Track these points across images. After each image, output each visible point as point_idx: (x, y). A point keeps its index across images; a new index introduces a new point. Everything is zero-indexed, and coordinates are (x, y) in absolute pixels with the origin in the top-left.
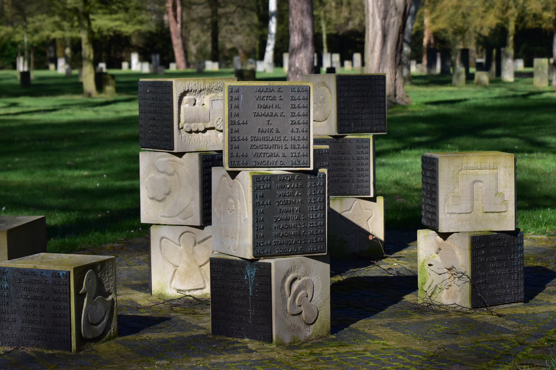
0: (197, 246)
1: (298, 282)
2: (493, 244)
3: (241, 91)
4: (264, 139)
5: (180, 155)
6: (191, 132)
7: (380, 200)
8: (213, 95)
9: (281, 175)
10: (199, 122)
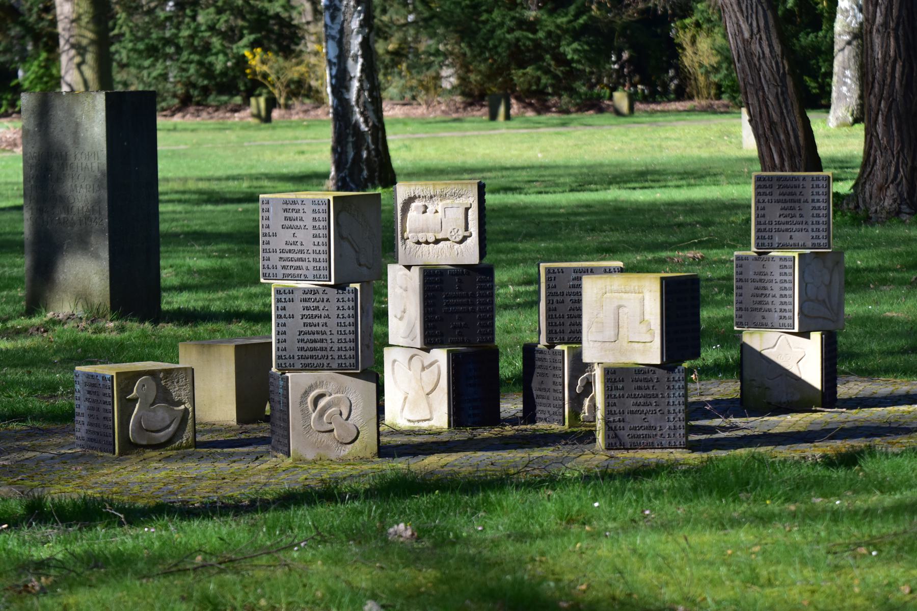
0: (426, 371)
3: (271, 203)
4: (290, 251)
6: (418, 243)
7: (816, 337)
8: (448, 201)
10: (428, 232)
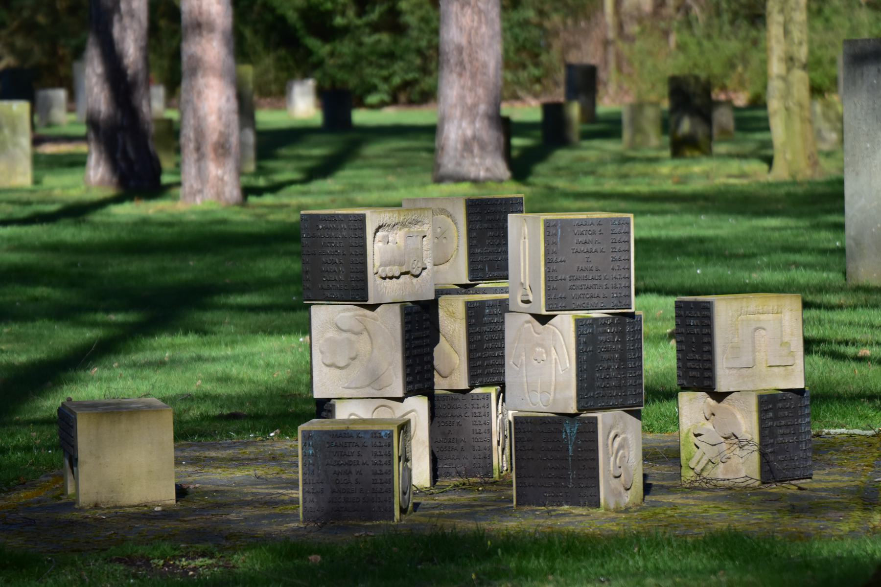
1: (618, 440)
2: (780, 405)
5: (373, 307)
9: (602, 318)
